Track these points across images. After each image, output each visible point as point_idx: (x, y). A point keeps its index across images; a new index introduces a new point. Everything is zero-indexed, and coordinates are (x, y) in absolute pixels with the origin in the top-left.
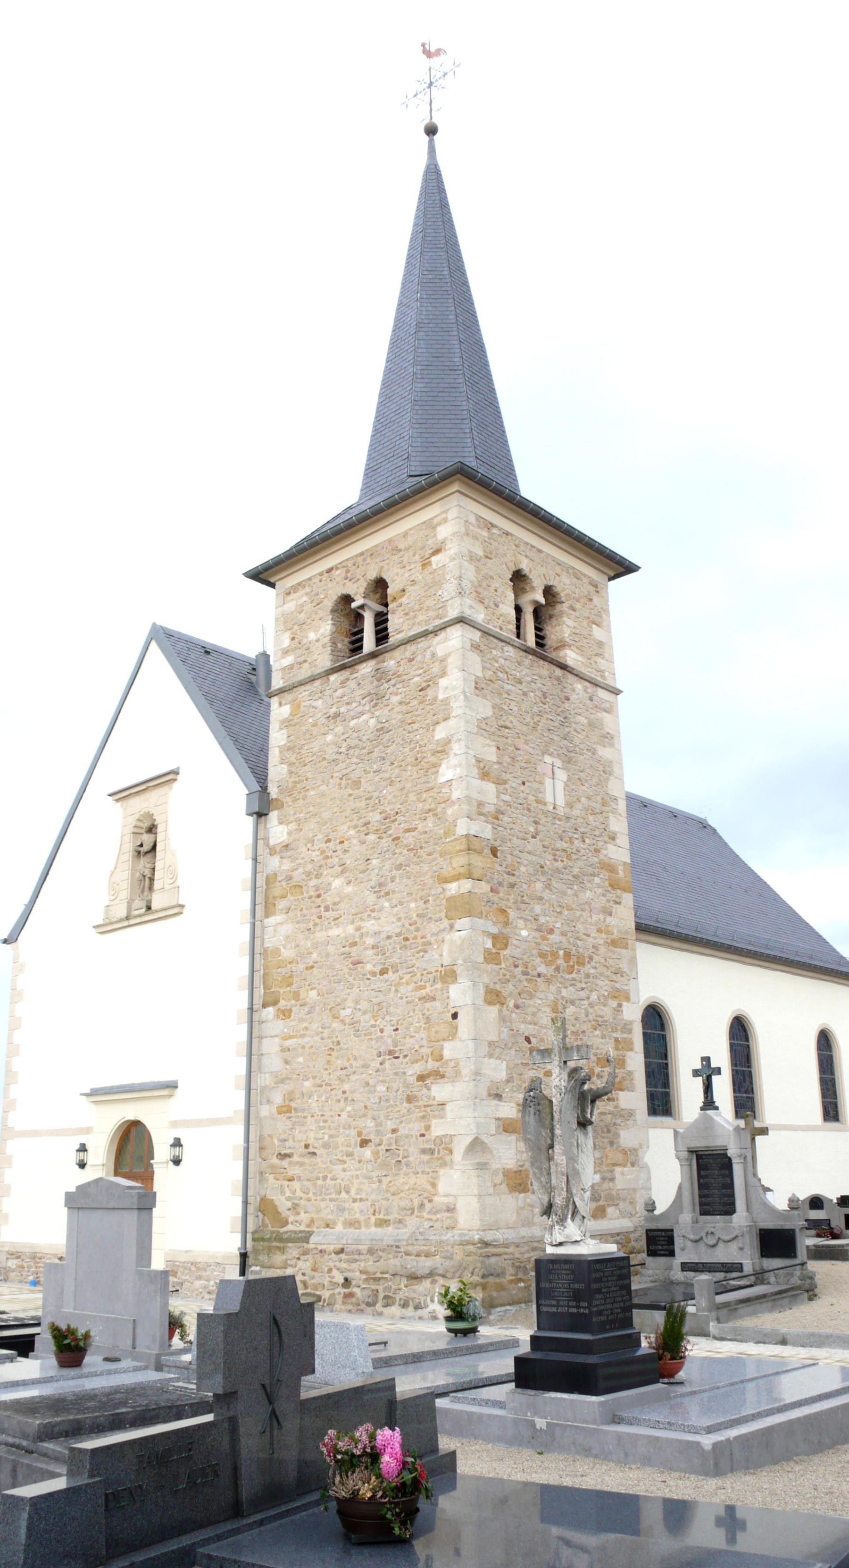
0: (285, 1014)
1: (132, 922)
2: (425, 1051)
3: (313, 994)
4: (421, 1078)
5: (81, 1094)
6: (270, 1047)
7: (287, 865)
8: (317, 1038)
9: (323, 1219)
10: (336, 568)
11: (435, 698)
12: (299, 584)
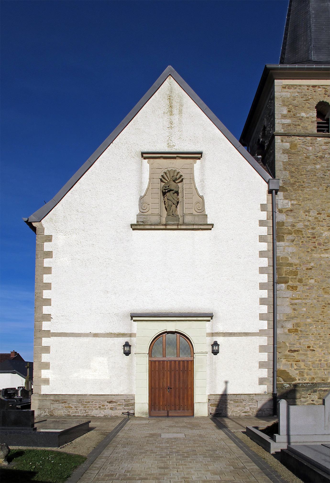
1: (168, 227)
3: (312, 281)
7: (291, 220)
8: (315, 301)
9: (320, 378)
10: (319, 86)
12: (292, 85)
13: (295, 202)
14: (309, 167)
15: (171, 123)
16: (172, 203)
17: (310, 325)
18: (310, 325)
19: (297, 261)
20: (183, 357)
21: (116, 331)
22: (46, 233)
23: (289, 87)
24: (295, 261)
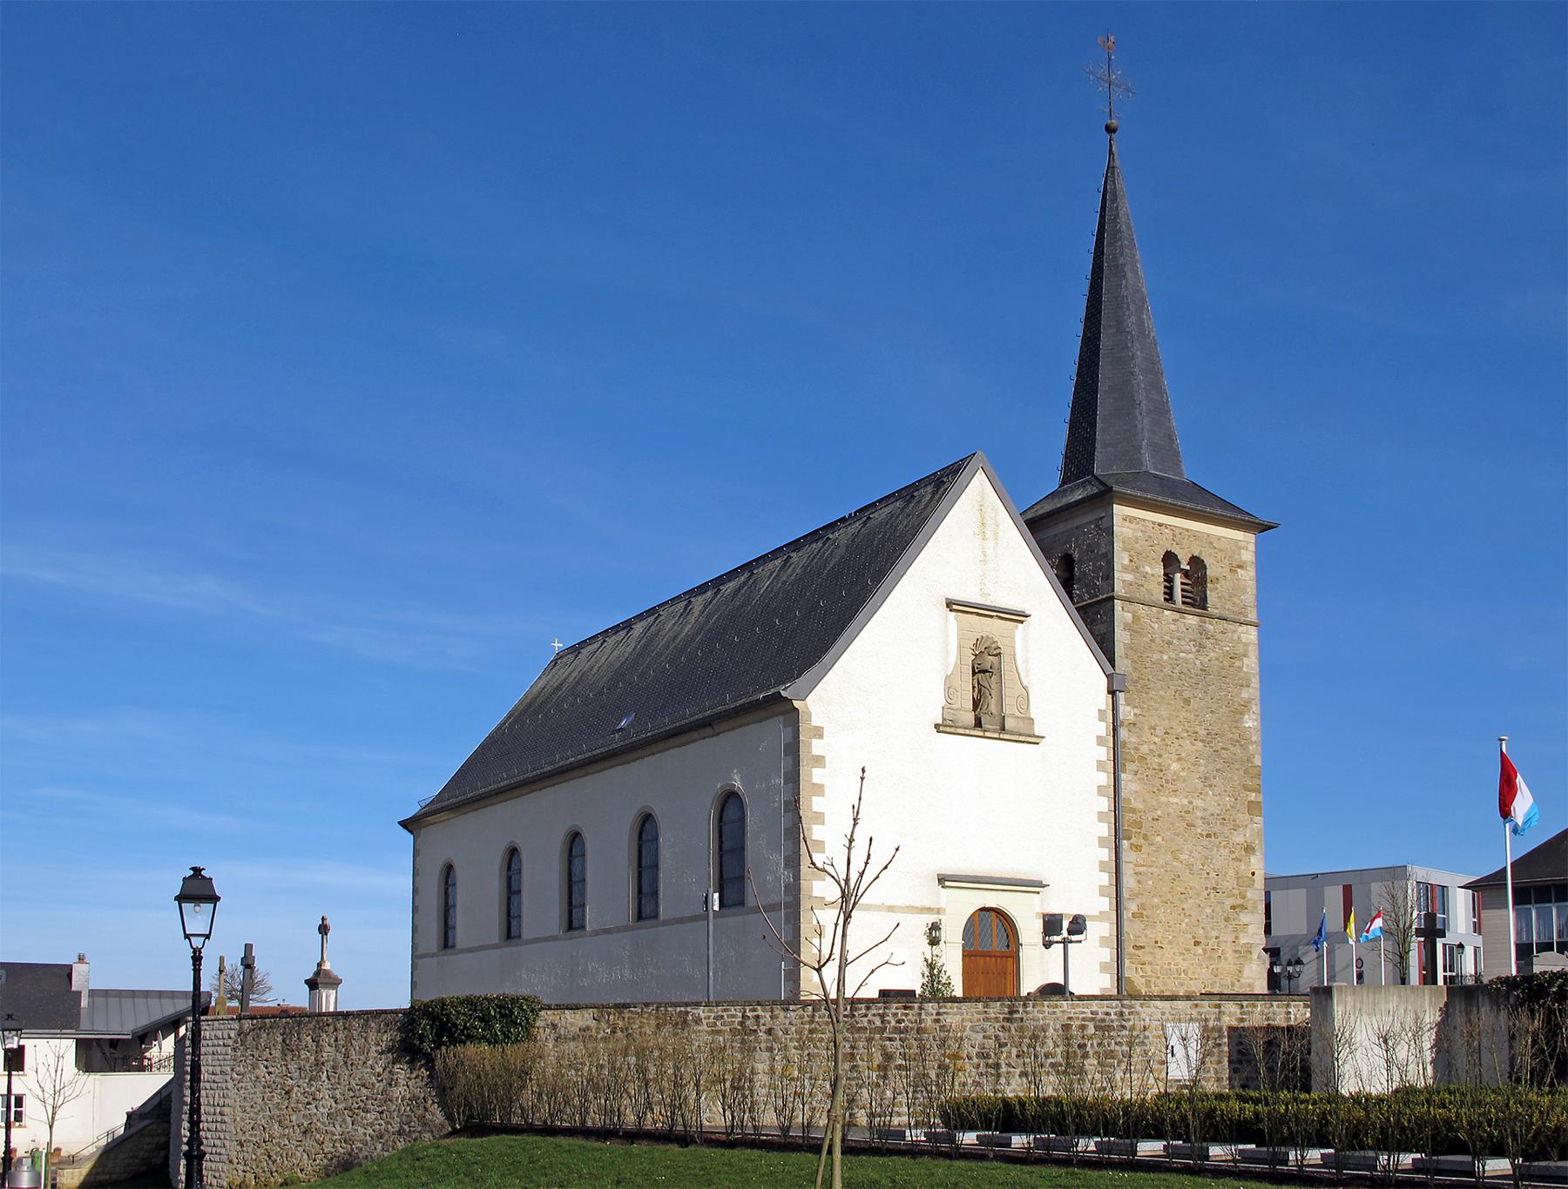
0: (1138, 848)
2: (1236, 892)
3: (1159, 839)
4: (1233, 907)
5: (248, 948)
6: (1127, 870)
7: (1134, 739)
11: (1241, 668)
13: (1137, 711)
14: (1155, 657)
15: (984, 553)
16: (985, 700)
17: (1157, 907)
18: (1157, 907)
19: (1141, 807)
20: (1040, 535)
21: (918, 904)
22: (815, 722)
23: (1132, 519)
24: (1139, 805)
